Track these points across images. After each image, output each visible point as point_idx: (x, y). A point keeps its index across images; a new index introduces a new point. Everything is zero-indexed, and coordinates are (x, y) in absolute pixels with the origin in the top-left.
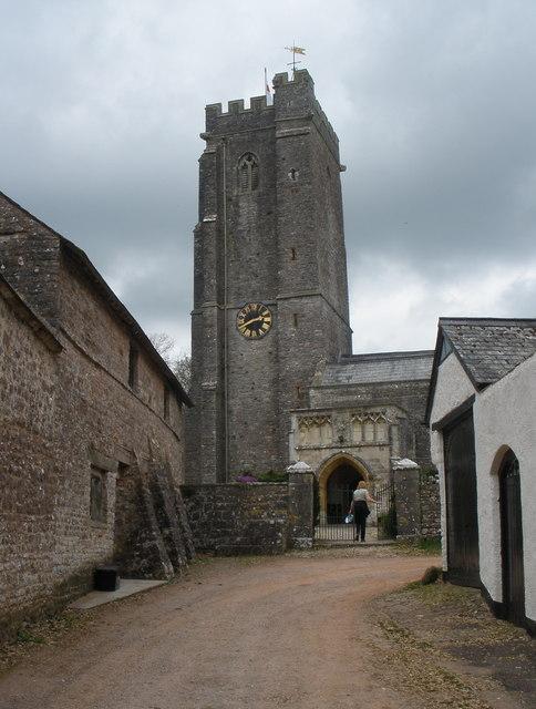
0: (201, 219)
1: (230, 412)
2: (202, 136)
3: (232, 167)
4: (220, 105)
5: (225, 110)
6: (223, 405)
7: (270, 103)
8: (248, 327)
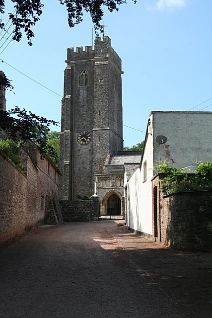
0: (65, 96)
1: (74, 172)
2: (66, 61)
3: (77, 75)
4: (73, 48)
5: (75, 51)
6: (72, 170)
7: (93, 49)
8: (82, 140)
